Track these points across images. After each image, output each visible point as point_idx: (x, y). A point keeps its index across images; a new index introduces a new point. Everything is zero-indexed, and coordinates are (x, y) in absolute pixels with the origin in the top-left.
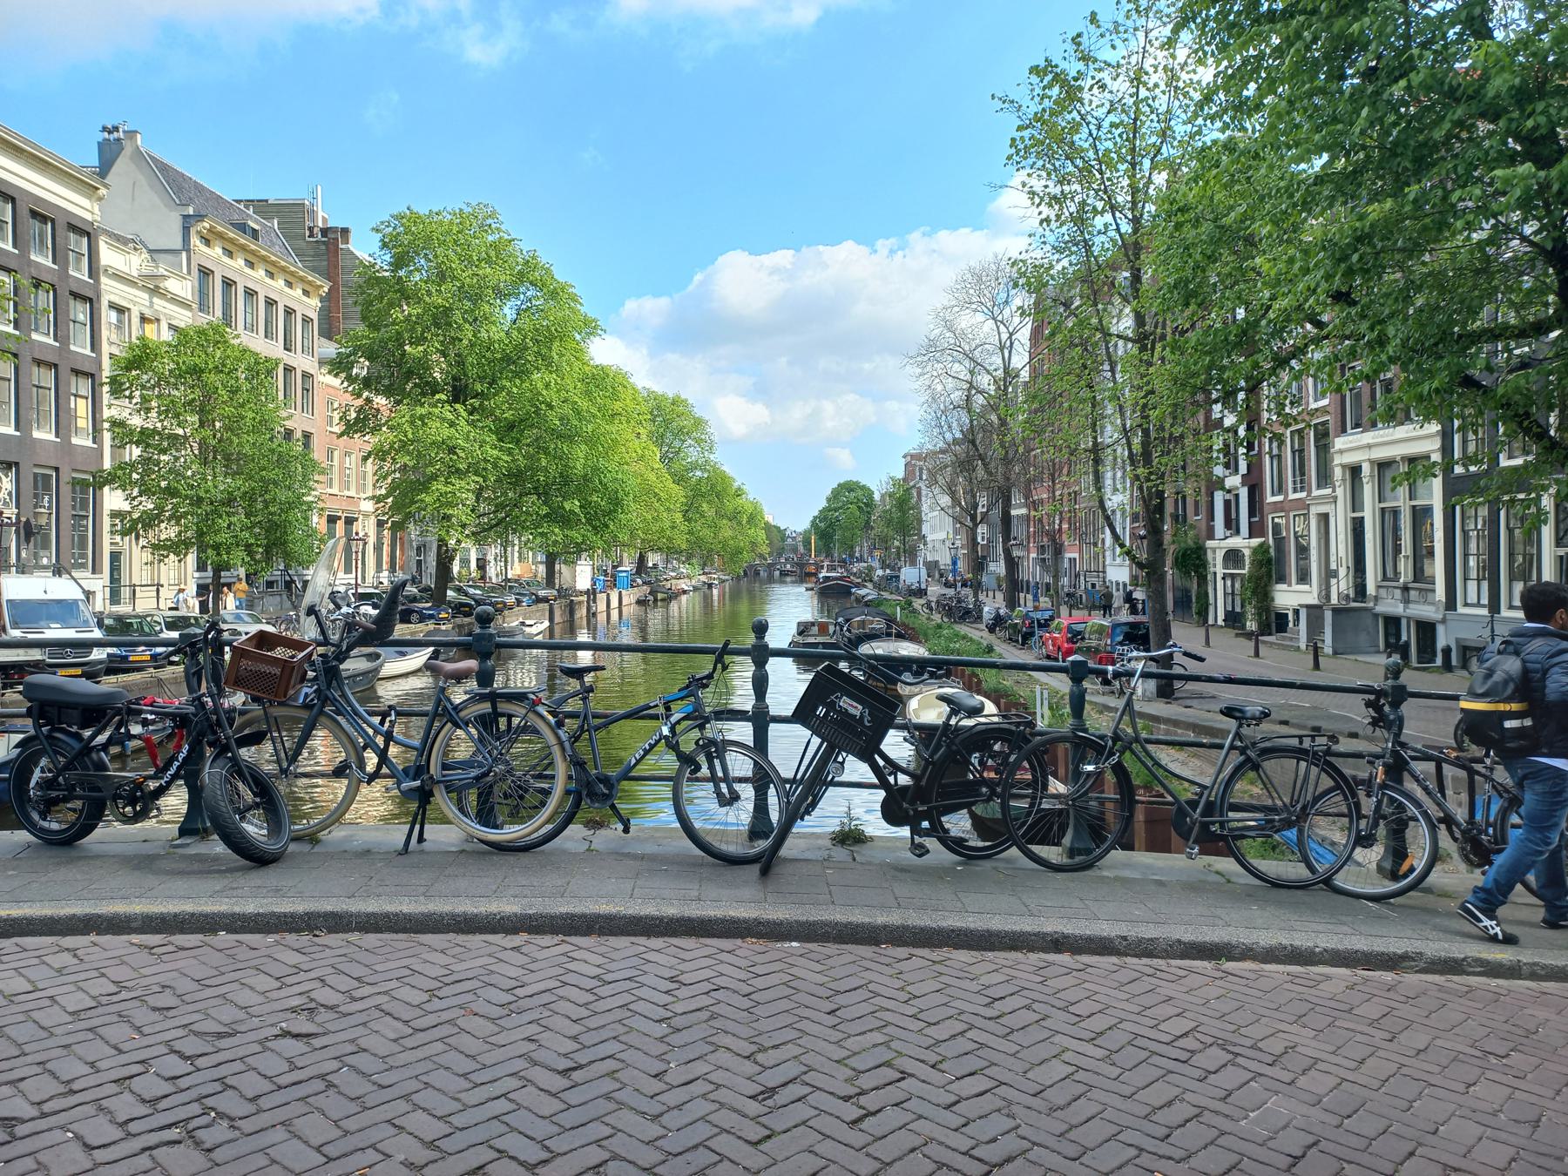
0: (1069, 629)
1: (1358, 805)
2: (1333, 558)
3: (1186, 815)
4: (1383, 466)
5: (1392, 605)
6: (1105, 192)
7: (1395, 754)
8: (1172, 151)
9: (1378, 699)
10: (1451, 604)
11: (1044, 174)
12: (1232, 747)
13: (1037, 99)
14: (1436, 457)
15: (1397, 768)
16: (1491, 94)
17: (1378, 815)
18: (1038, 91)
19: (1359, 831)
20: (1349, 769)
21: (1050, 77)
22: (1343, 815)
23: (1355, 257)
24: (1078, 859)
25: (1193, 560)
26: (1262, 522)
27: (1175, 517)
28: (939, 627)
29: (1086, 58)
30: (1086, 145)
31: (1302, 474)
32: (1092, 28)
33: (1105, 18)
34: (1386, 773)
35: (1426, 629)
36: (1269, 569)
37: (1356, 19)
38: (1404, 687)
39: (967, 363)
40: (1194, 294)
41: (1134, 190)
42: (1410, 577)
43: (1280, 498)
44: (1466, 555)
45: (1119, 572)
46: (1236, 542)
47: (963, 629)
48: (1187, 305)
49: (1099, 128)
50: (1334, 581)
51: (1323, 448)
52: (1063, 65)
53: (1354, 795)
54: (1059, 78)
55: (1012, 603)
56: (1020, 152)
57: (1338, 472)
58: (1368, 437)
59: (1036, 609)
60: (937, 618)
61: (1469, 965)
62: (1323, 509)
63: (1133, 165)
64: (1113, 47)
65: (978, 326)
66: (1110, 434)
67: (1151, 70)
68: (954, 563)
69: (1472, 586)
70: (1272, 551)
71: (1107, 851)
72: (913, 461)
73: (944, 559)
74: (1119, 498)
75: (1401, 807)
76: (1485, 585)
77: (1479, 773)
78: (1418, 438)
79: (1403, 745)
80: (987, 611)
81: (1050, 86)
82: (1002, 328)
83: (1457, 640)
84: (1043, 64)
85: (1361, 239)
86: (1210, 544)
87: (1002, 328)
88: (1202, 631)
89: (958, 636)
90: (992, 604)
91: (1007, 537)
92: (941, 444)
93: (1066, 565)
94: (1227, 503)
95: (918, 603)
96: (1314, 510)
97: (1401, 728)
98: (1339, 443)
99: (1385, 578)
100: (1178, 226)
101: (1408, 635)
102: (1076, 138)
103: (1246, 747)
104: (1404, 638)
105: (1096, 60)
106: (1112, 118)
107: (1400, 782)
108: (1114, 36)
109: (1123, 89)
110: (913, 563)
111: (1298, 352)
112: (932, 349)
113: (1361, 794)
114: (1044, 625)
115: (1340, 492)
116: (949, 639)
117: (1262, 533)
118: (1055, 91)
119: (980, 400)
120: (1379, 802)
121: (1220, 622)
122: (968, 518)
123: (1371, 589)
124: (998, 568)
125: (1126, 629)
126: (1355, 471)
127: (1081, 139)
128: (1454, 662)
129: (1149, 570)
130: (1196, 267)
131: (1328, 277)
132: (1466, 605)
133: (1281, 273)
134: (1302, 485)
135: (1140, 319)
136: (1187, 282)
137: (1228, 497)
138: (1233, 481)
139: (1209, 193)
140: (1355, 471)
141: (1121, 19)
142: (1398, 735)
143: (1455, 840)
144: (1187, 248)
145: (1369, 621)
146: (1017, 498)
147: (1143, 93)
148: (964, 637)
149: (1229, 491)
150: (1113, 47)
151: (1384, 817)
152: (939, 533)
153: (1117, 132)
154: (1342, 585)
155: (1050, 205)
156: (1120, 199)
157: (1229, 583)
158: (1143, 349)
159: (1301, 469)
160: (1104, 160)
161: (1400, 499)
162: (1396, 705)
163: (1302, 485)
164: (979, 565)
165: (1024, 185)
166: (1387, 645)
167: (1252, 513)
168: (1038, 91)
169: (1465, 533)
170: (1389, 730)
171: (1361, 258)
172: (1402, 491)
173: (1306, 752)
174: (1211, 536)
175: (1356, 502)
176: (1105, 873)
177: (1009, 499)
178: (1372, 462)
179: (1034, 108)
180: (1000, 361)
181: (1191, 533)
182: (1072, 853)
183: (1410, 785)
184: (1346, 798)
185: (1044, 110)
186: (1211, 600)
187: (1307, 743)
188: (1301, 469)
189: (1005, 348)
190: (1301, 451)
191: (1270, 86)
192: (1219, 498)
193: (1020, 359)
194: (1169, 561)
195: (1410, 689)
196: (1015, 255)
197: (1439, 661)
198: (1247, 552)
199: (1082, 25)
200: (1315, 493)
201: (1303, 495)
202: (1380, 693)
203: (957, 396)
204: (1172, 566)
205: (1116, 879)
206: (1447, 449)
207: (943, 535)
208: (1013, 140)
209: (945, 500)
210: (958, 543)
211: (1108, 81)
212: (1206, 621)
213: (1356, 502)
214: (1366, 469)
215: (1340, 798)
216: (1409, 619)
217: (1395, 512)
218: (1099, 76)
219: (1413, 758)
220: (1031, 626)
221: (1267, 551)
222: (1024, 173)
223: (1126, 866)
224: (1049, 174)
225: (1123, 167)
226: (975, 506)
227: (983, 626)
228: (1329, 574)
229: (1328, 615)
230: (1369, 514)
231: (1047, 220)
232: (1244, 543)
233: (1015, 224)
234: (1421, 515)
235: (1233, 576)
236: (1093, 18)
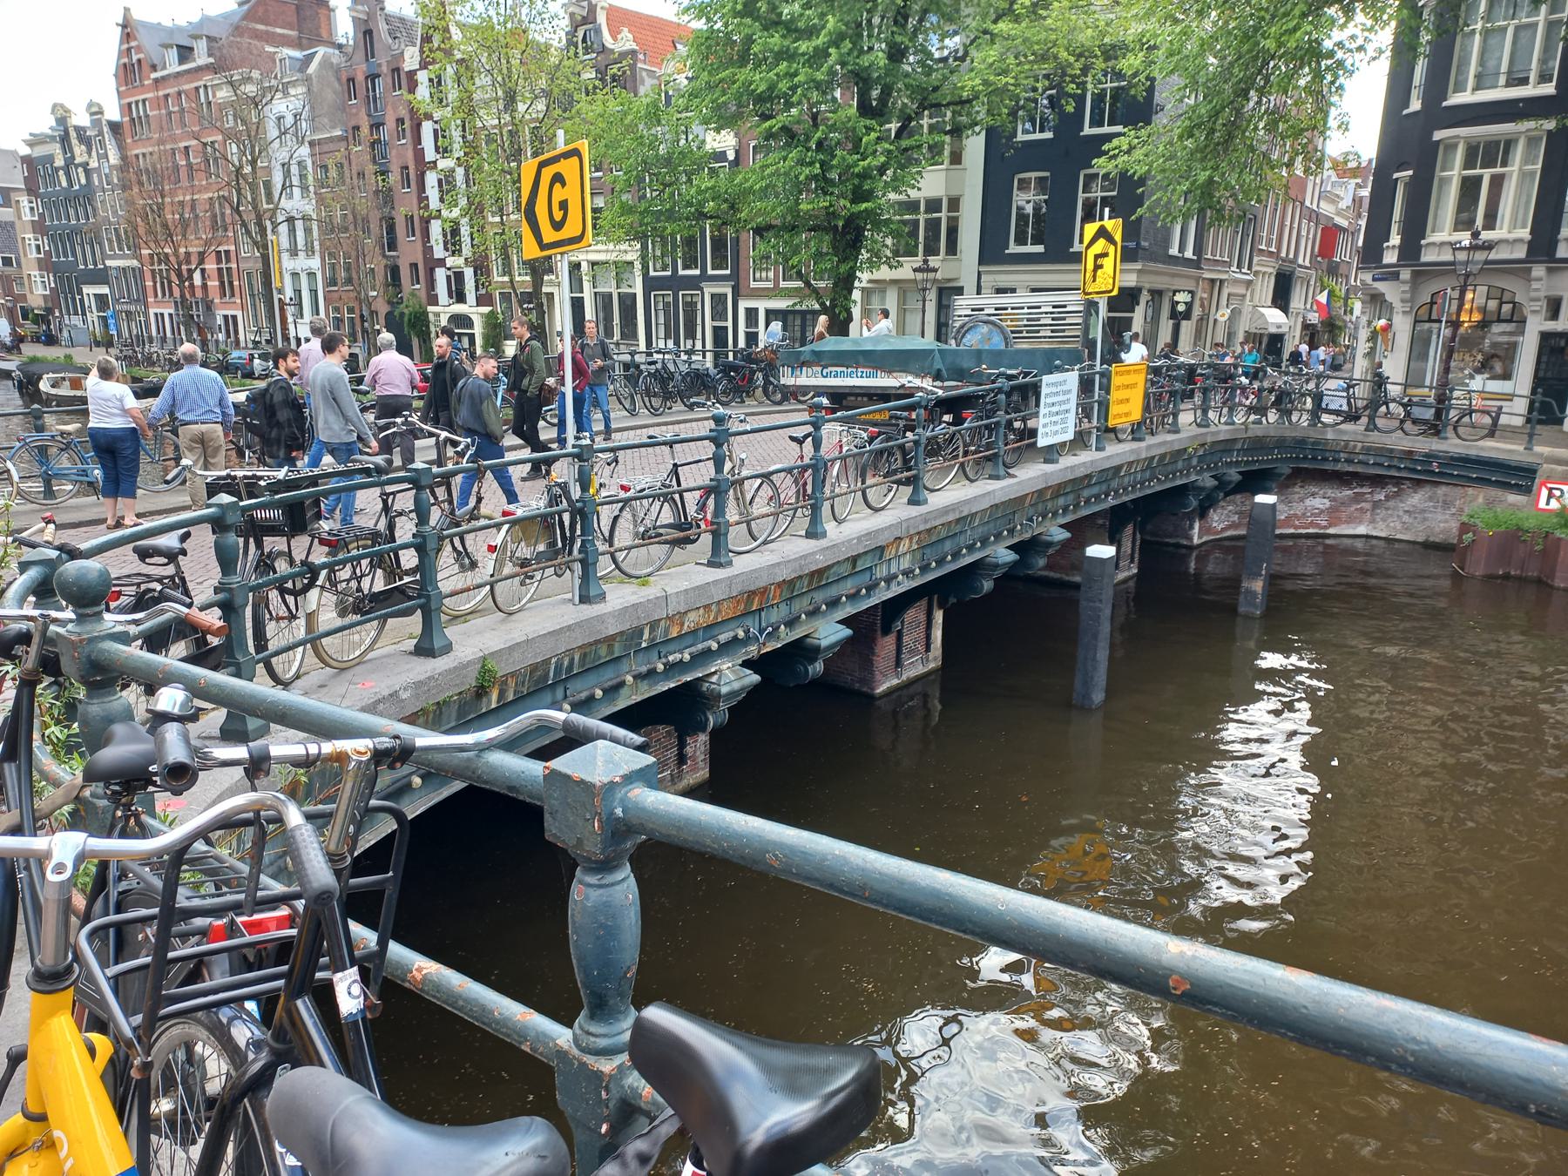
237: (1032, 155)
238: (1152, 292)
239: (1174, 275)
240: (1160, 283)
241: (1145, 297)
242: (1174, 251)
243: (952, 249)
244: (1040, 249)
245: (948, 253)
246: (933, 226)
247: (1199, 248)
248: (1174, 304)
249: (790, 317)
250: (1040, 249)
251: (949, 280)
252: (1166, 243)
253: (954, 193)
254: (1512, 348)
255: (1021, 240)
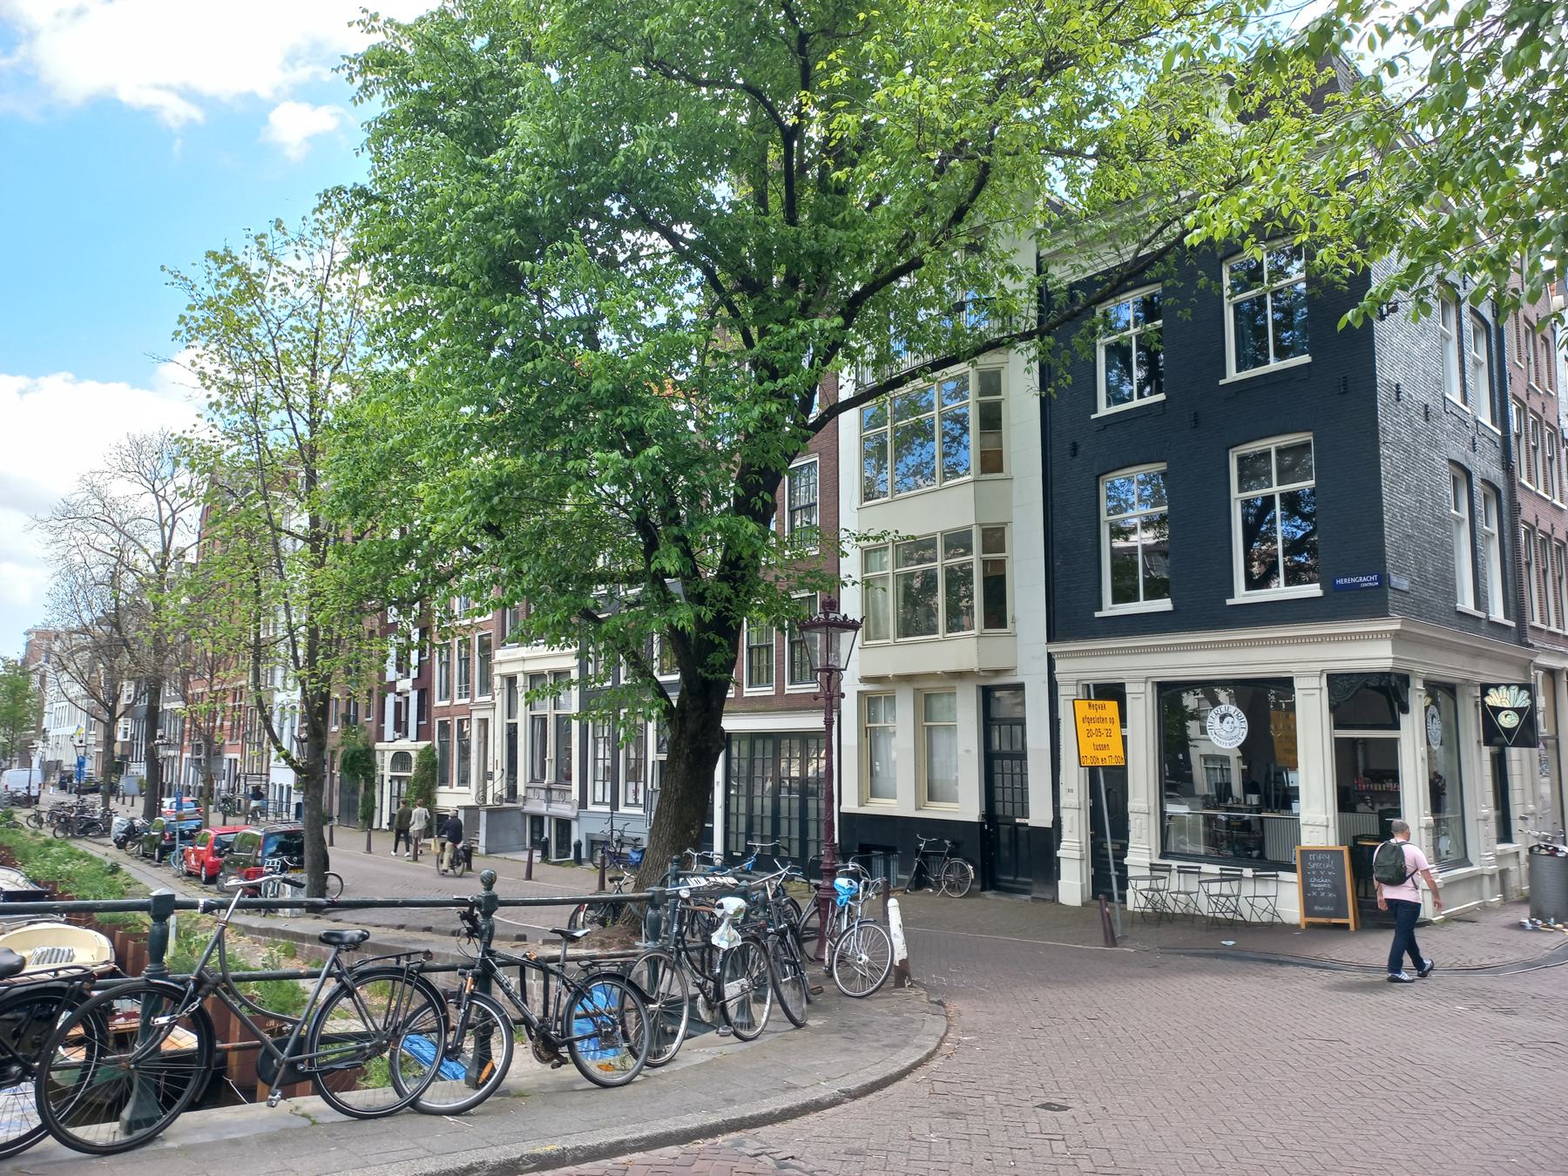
0: (217, 841)
1: (447, 1019)
2: (490, 761)
3: (272, 1056)
4: (534, 677)
5: (537, 806)
6: (283, 389)
7: (484, 962)
8: (351, 367)
9: (471, 911)
10: (583, 803)
11: (218, 359)
12: (329, 974)
13: (213, 284)
14: (575, 675)
15: (485, 977)
16: (594, 392)
17: (466, 1025)
18: (215, 275)
19: (446, 1044)
20: (440, 980)
21: (229, 266)
22: (432, 1031)
23: (496, 500)
24: (138, 1133)
25: (361, 764)
26: (429, 726)
27: (346, 718)
28: (49, 844)
29: (269, 259)
30: (266, 341)
31: (467, 681)
32: (276, 234)
33: (293, 226)
34: (475, 982)
35: (564, 825)
36: (433, 772)
37: (498, 303)
38: (495, 897)
39: (116, 536)
40: (362, 505)
41: (313, 396)
42: (553, 779)
43: (447, 703)
44: (596, 759)
45: (283, 775)
46: (405, 744)
47: (82, 846)
48: (356, 514)
49: (279, 327)
50: (489, 783)
51: (486, 659)
52: (242, 259)
53: (444, 1009)
54: (239, 270)
55: (152, 810)
56: (189, 330)
57: (497, 681)
58: (523, 651)
59: (180, 818)
60: (47, 832)
61: (525, 1163)
62: (483, 715)
63: (314, 372)
64: (298, 258)
65: (131, 494)
66: (275, 628)
67: (334, 289)
68: (81, 764)
69: (599, 786)
70: (437, 754)
71: (175, 1116)
72: (40, 641)
73: (69, 760)
74: (287, 696)
75: (487, 1015)
76: (608, 785)
77: (552, 972)
78: (565, 659)
79: (491, 953)
80: (118, 823)
81: (229, 274)
82: (164, 504)
83: (587, 835)
84: (221, 252)
85: (500, 485)
86: (379, 746)
87: (164, 504)
88: (364, 836)
89: (72, 854)
90: (127, 812)
91: (151, 735)
92: (75, 625)
93: (225, 766)
94: (398, 705)
95: (21, 815)
96: (476, 715)
97: (491, 938)
98: (499, 655)
99: (533, 780)
100: (349, 440)
101: (550, 832)
102: (254, 331)
103: (343, 974)
104: (546, 835)
105: (278, 265)
106: (292, 322)
107: (487, 990)
108: (299, 247)
109: (306, 298)
110: (26, 763)
111: (456, 572)
112: (70, 513)
113: (451, 1008)
114: (186, 837)
115: (498, 699)
116: (59, 860)
117: (429, 737)
118: (234, 281)
119: (130, 580)
120: (467, 1013)
121: (385, 826)
122: (106, 711)
123: (521, 791)
124: (139, 769)
125: (281, 838)
126: (511, 680)
127: (259, 332)
128: (584, 856)
129: (310, 776)
130: (366, 481)
131: (475, 512)
132: (595, 803)
133: (436, 503)
134: (466, 692)
135: (314, 521)
136: (356, 494)
137: (399, 699)
138: (405, 684)
139: (382, 415)
140: (511, 680)
141: (307, 234)
142: (488, 944)
143: (531, 1038)
144: (357, 461)
145: (518, 819)
146: (167, 692)
147: (326, 307)
148: (82, 856)
149: (399, 694)
150: (298, 258)
151: (471, 1026)
152: (66, 729)
153: (297, 336)
154: (497, 786)
155: (222, 392)
156: (298, 399)
157: (396, 784)
158: (315, 549)
159: (466, 678)
160: (282, 359)
161: (546, 708)
162: (487, 915)
163: (466, 692)
164: (114, 766)
165: (193, 364)
166: (533, 842)
167: (420, 717)
168: (215, 275)
169: (595, 739)
170: (481, 938)
171: (501, 501)
172: (549, 701)
173: (402, 970)
174: (381, 738)
175: (511, 712)
176: (169, 1144)
177: (157, 693)
178: (525, 673)
179: (210, 291)
180: (158, 539)
181: (362, 735)
182: (130, 1128)
183: (498, 994)
184: (436, 1014)
185: (221, 296)
186: (378, 804)
187: (404, 963)
188: (466, 678)
189: (167, 525)
190: (467, 660)
191: (432, 336)
192: (390, 700)
193: (185, 538)
194: (337, 765)
195: (501, 898)
196: (179, 433)
197: (572, 856)
198: (414, 755)
199: (266, 228)
200: (478, 699)
201: (467, 701)
202: (472, 905)
203: (100, 572)
204: (337, 773)
205: (180, 1149)
206: (583, 668)
207: (71, 730)
208: (182, 317)
209: (76, 690)
210: (92, 740)
211: (291, 286)
212: (371, 826)
213: (511, 712)
214: (520, 679)
215: (431, 1014)
216: (550, 817)
217: (544, 720)
218: (281, 279)
219: (499, 965)
220: (172, 839)
221: (433, 754)
222: (193, 352)
223: (199, 1129)
224: (223, 359)
225: (302, 370)
226: (116, 698)
227: (110, 841)
228: (488, 776)
229: (483, 815)
230: (522, 718)
231: (218, 404)
232: (411, 745)
233: (178, 399)
234: (563, 723)
235: (400, 779)
236: (278, 224)
237: (1129, 440)
238: (1433, 687)
239: (1477, 654)
240: (1448, 668)
241: (1417, 699)
242: (1467, 603)
243: (996, 615)
244: (1165, 604)
245: (989, 623)
246: (958, 578)
247: (1515, 604)
248: (1490, 715)
249: (759, 744)
250: (1165, 604)
251: (997, 672)
252: (1451, 594)
253: (993, 519)
254: (972, 607)
255: (1121, 596)
